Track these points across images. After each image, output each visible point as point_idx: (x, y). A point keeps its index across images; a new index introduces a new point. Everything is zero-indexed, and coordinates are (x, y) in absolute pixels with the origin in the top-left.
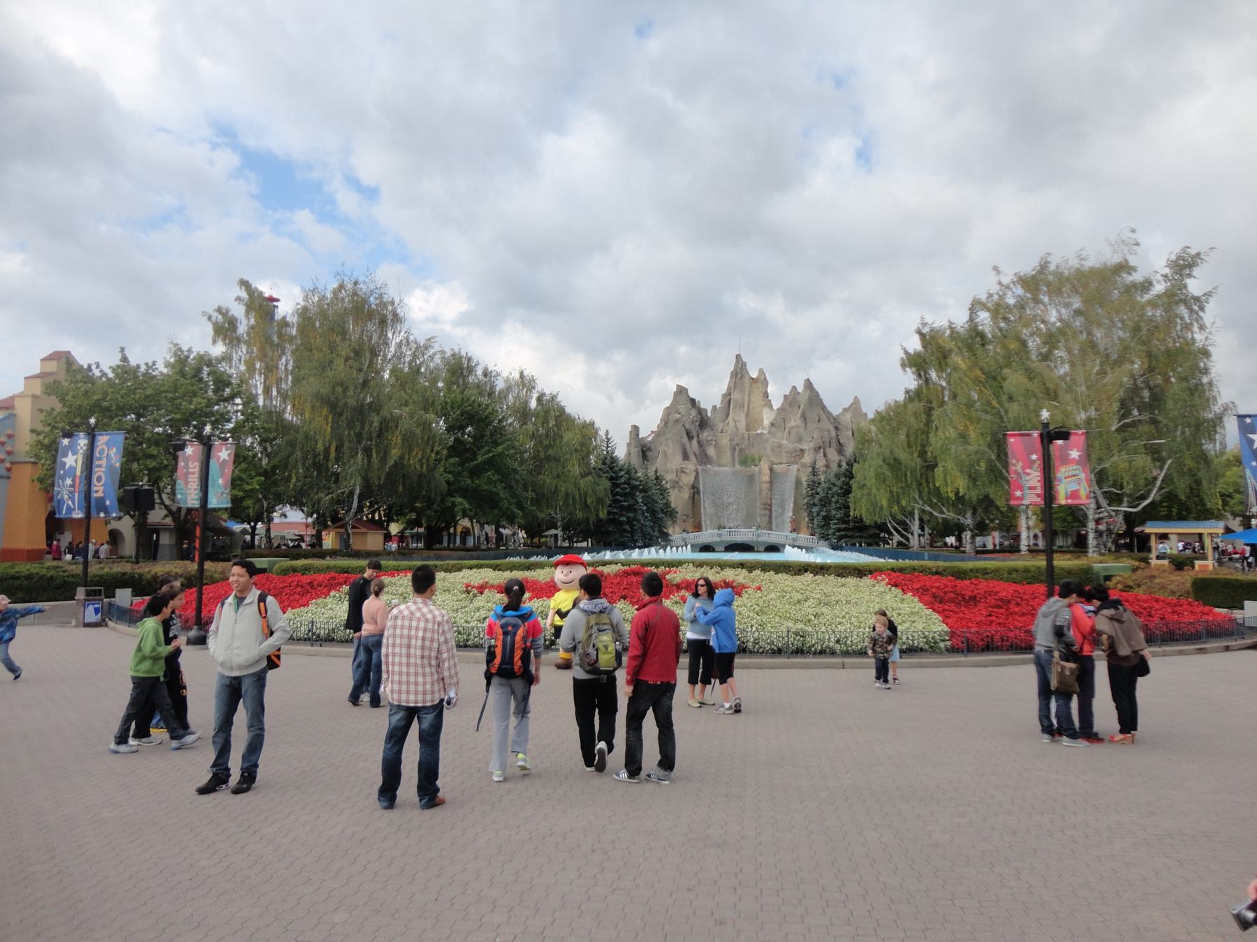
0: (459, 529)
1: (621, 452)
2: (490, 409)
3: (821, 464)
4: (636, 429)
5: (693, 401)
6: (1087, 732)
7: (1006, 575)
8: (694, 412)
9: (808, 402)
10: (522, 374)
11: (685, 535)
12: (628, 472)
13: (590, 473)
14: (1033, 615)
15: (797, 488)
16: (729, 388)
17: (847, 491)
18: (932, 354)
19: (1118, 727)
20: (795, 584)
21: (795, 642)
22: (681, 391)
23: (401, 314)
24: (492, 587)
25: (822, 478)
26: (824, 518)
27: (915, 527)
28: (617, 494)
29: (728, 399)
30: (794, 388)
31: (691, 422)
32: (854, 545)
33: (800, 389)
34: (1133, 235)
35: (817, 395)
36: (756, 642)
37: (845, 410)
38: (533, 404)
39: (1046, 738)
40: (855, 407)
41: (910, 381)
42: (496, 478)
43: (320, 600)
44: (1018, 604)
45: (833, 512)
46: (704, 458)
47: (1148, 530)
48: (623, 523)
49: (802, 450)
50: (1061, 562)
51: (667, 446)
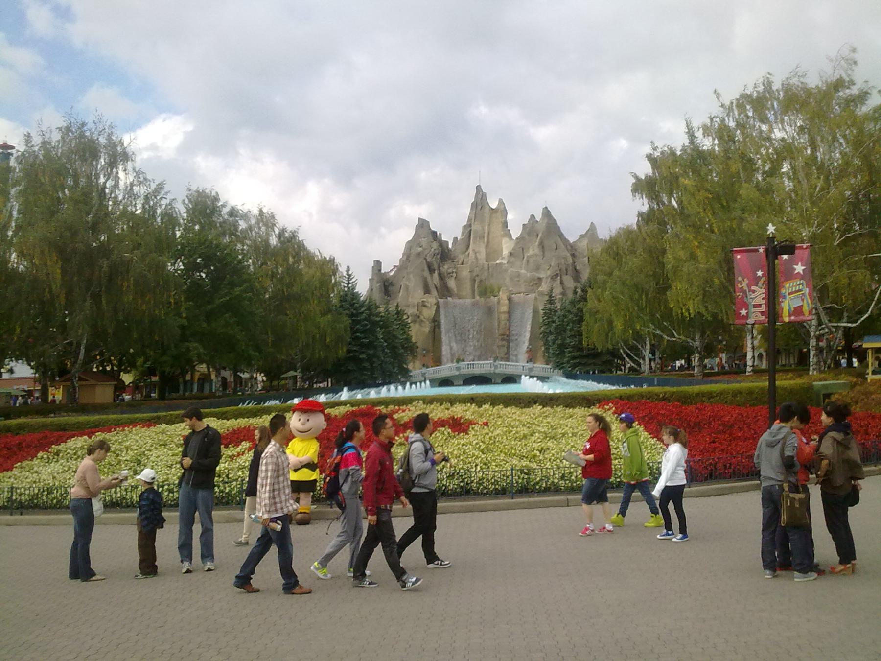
0: (197, 375)
1: (362, 287)
3: (557, 291)
4: (378, 264)
5: (434, 233)
6: (806, 563)
8: (435, 245)
9: (545, 231)
10: (261, 211)
11: (424, 370)
12: (369, 309)
13: (330, 311)
14: (755, 439)
15: (534, 317)
16: (469, 220)
17: (581, 320)
18: (667, 176)
19: (838, 559)
20: (523, 418)
21: (519, 480)
22: (423, 224)
25: (559, 305)
27: (647, 353)
28: (357, 331)
29: (468, 230)
31: (432, 256)
32: (588, 372)
33: (538, 217)
34: (852, 55)
35: (555, 222)
37: (582, 236)
38: (274, 241)
39: (768, 575)
40: (592, 230)
41: (642, 205)
42: (233, 320)
43: (25, 463)
44: (741, 429)
45: (568, 340)
46: (445, 291)
47: (865, 346)
48: (362, 360)
49: (540, 279)
50: (784, 382)
51: (409, 280)
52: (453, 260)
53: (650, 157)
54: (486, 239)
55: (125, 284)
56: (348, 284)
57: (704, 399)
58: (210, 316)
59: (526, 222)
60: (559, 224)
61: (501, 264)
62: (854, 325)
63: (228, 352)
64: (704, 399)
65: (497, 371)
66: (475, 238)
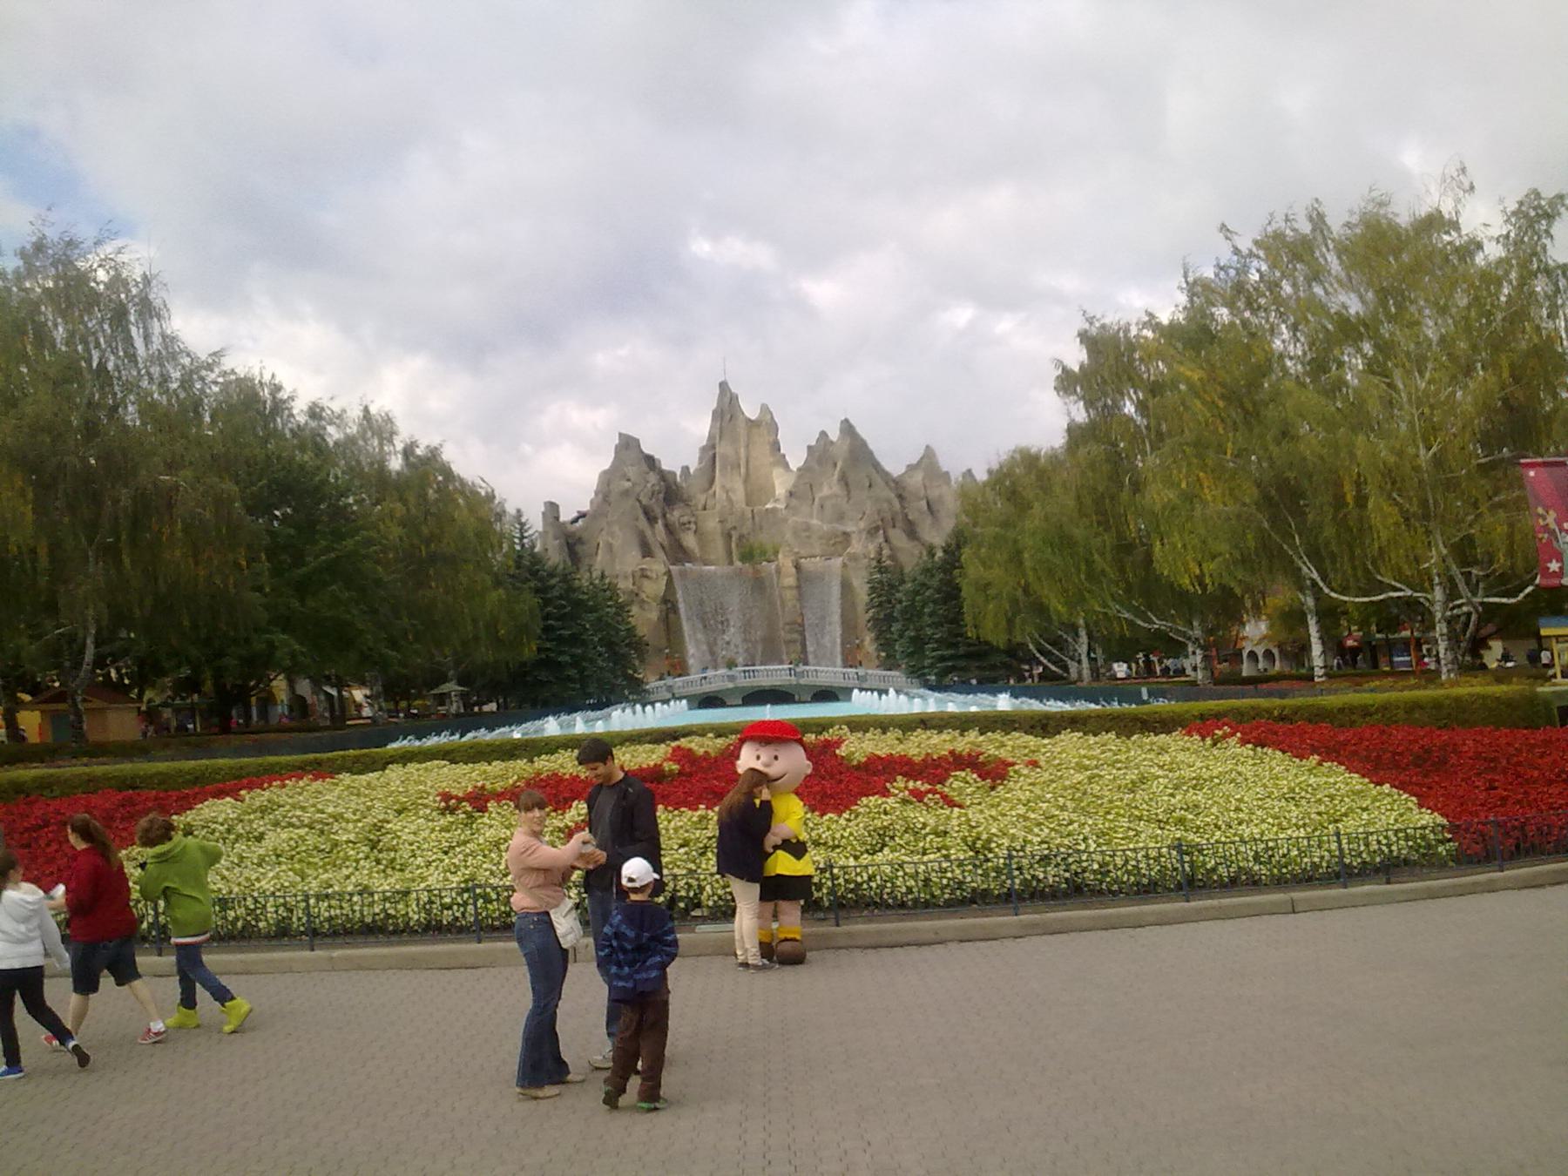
2: (323, 475)
7: (1401, 713)
8: (653, 478)
9: (847, 457)
16: (711, 437)
18: (1108, 364)
22: (628, 444)
23: (157, 303)
24: (499, 796)
26: (913, 640)
29: (710, 455)
30: (823, 434)
31: (650, 495)
33: (834, 435)
35: (864, 444)
36: (1104, 871)
38: (395, 464)
40: (928, 463)
45: (929, 631)
46: (678, 553)
49: (846, 535)
51: (612, 534)
52: (686, 502)
53: (1084, 337)
54: (743, 470)
55: (166, 530)
56: (522, 538)
57: (1354, 717)
58: (302, 588)
59: (813, 443)
60: (871, 446)
61: (774, 510)
62: (1512, 601)
63: (334, 649)
64: (1354, 717)
65: (802, 681)
66: (724, 468)
